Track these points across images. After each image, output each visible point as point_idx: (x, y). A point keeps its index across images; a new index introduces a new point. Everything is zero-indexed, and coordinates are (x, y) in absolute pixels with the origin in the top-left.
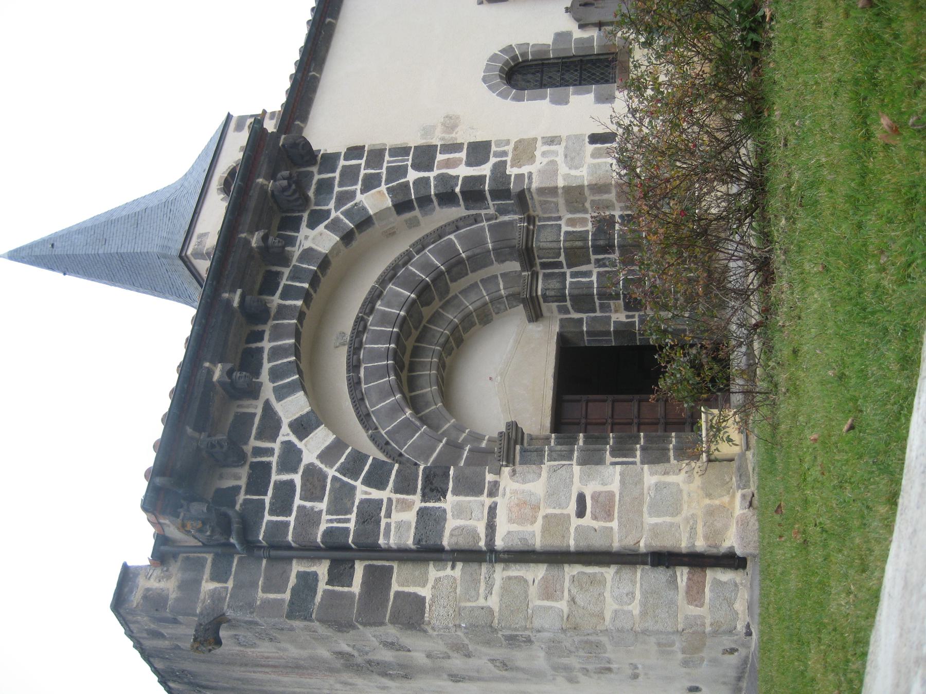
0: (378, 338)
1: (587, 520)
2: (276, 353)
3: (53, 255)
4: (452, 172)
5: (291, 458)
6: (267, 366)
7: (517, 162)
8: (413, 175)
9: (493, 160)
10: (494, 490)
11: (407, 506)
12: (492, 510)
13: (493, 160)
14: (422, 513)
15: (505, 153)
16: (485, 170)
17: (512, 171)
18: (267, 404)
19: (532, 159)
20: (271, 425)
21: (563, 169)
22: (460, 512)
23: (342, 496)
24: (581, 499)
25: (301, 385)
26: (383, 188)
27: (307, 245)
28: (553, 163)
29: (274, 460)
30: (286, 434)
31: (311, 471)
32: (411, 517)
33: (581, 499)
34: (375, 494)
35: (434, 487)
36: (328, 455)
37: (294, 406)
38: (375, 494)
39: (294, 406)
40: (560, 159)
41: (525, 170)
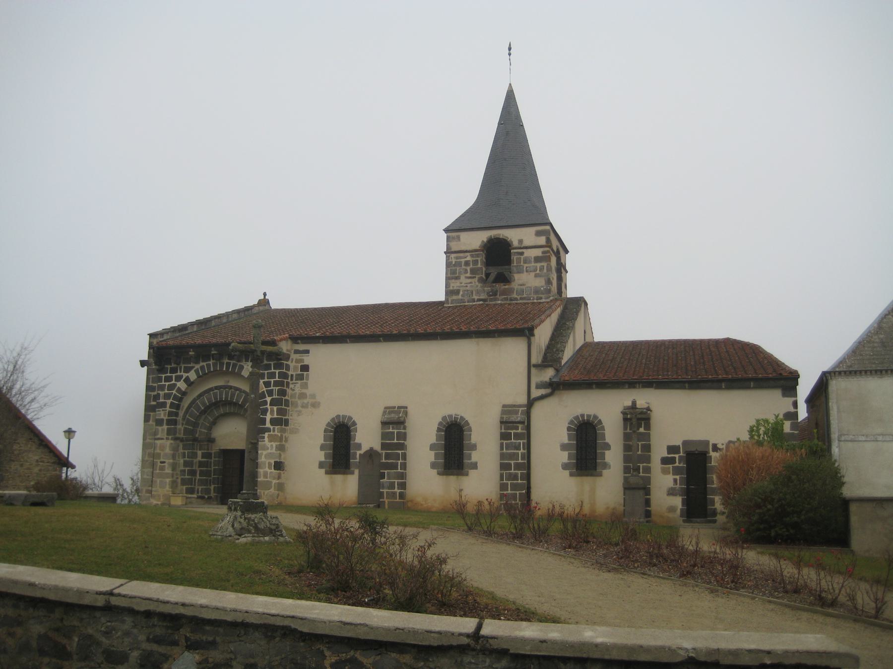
0: (227, 394)
1: (159, 464)
2: (209, 366)
3: (510, 98)
4: (268, 414)
5: (178, 379)
6: (205, 364)
7: (269, 436)
8: (268, 399)
9: (272, 427)
10: (167, 439)
11: (165, 415)
12: (162, 439)
13: (272, 427)
14: (162, 420)
15: (274, 431)
16: (268, 425)
17: (266, 435)
18: (193, 367)
19: (270, 441)
20: (187, 370)
21: (265, 453)
22: (163, 430)
23: (167, 396)
24: (164, 462)
25: (199, 377)
26: (265, 389)
27: (245, 367)
28: (268, 449)
29: (179, 374)
30: (185, 375)
31: (175, 385)
32: (162, 417)
33: (164, 462)
34: (168, 406)
35: (169, 422)
36: (179, 390)
37: (192, 376)
38: (168, 406)
39: (192, 376)
40: (269, 451)
41: (266, 439)
